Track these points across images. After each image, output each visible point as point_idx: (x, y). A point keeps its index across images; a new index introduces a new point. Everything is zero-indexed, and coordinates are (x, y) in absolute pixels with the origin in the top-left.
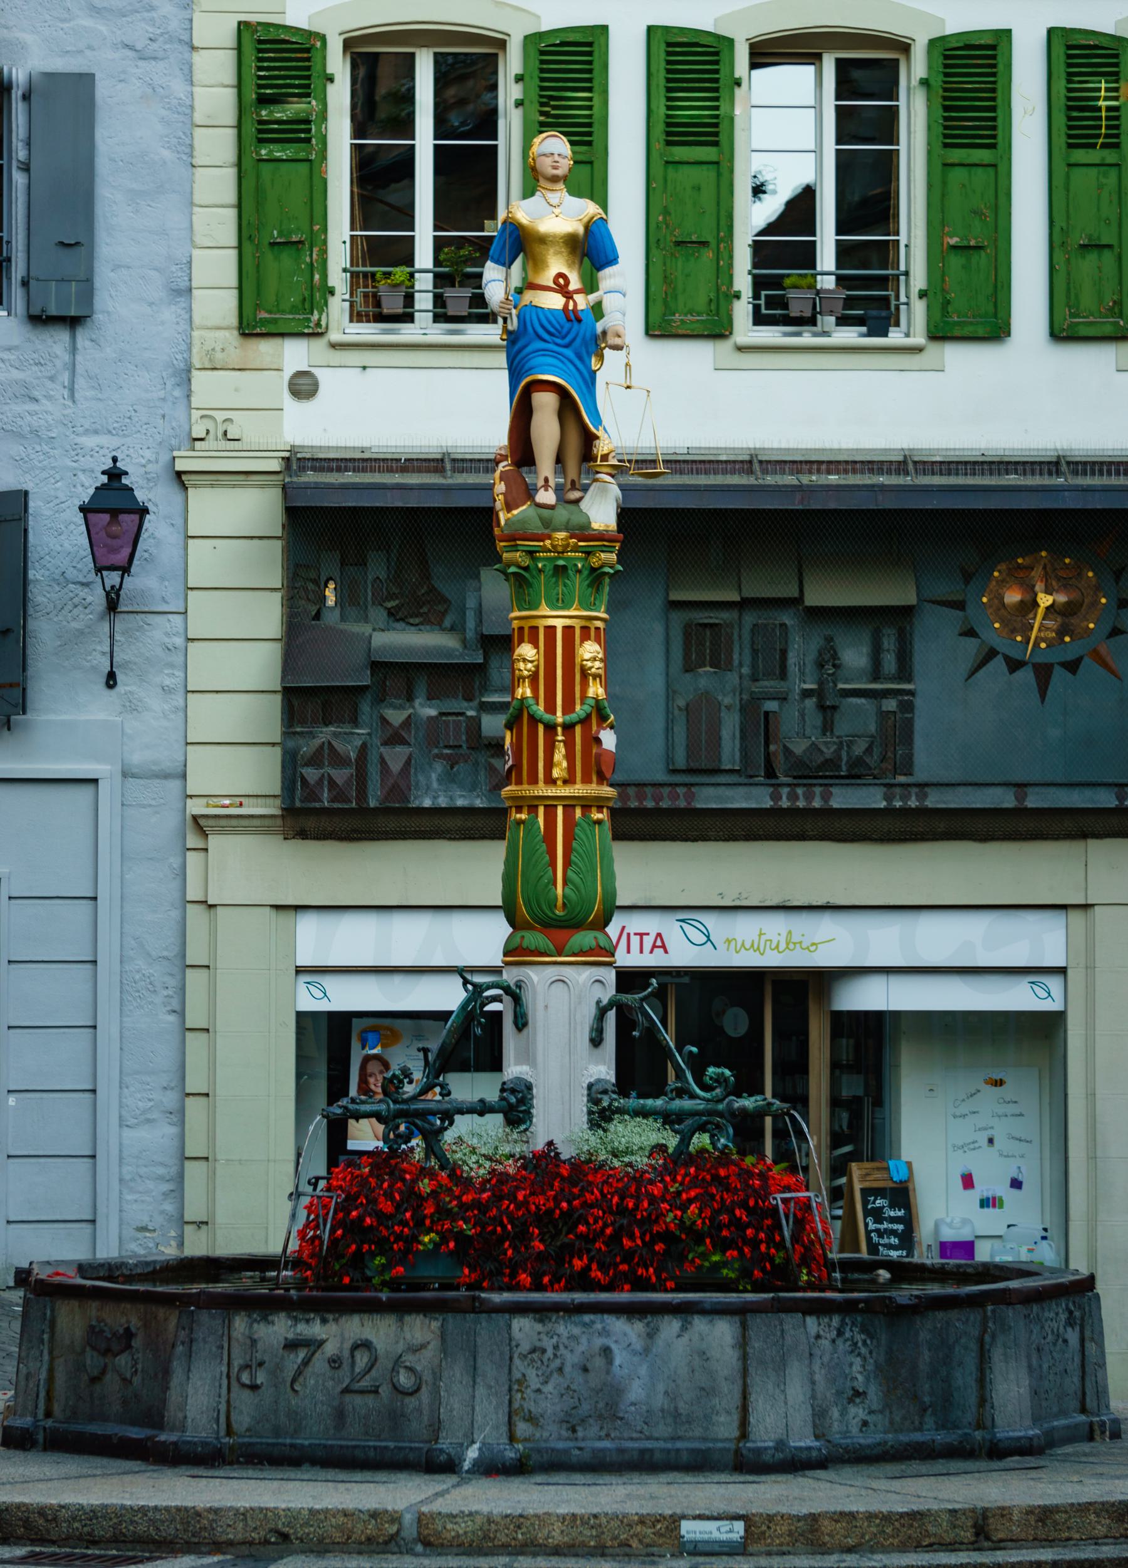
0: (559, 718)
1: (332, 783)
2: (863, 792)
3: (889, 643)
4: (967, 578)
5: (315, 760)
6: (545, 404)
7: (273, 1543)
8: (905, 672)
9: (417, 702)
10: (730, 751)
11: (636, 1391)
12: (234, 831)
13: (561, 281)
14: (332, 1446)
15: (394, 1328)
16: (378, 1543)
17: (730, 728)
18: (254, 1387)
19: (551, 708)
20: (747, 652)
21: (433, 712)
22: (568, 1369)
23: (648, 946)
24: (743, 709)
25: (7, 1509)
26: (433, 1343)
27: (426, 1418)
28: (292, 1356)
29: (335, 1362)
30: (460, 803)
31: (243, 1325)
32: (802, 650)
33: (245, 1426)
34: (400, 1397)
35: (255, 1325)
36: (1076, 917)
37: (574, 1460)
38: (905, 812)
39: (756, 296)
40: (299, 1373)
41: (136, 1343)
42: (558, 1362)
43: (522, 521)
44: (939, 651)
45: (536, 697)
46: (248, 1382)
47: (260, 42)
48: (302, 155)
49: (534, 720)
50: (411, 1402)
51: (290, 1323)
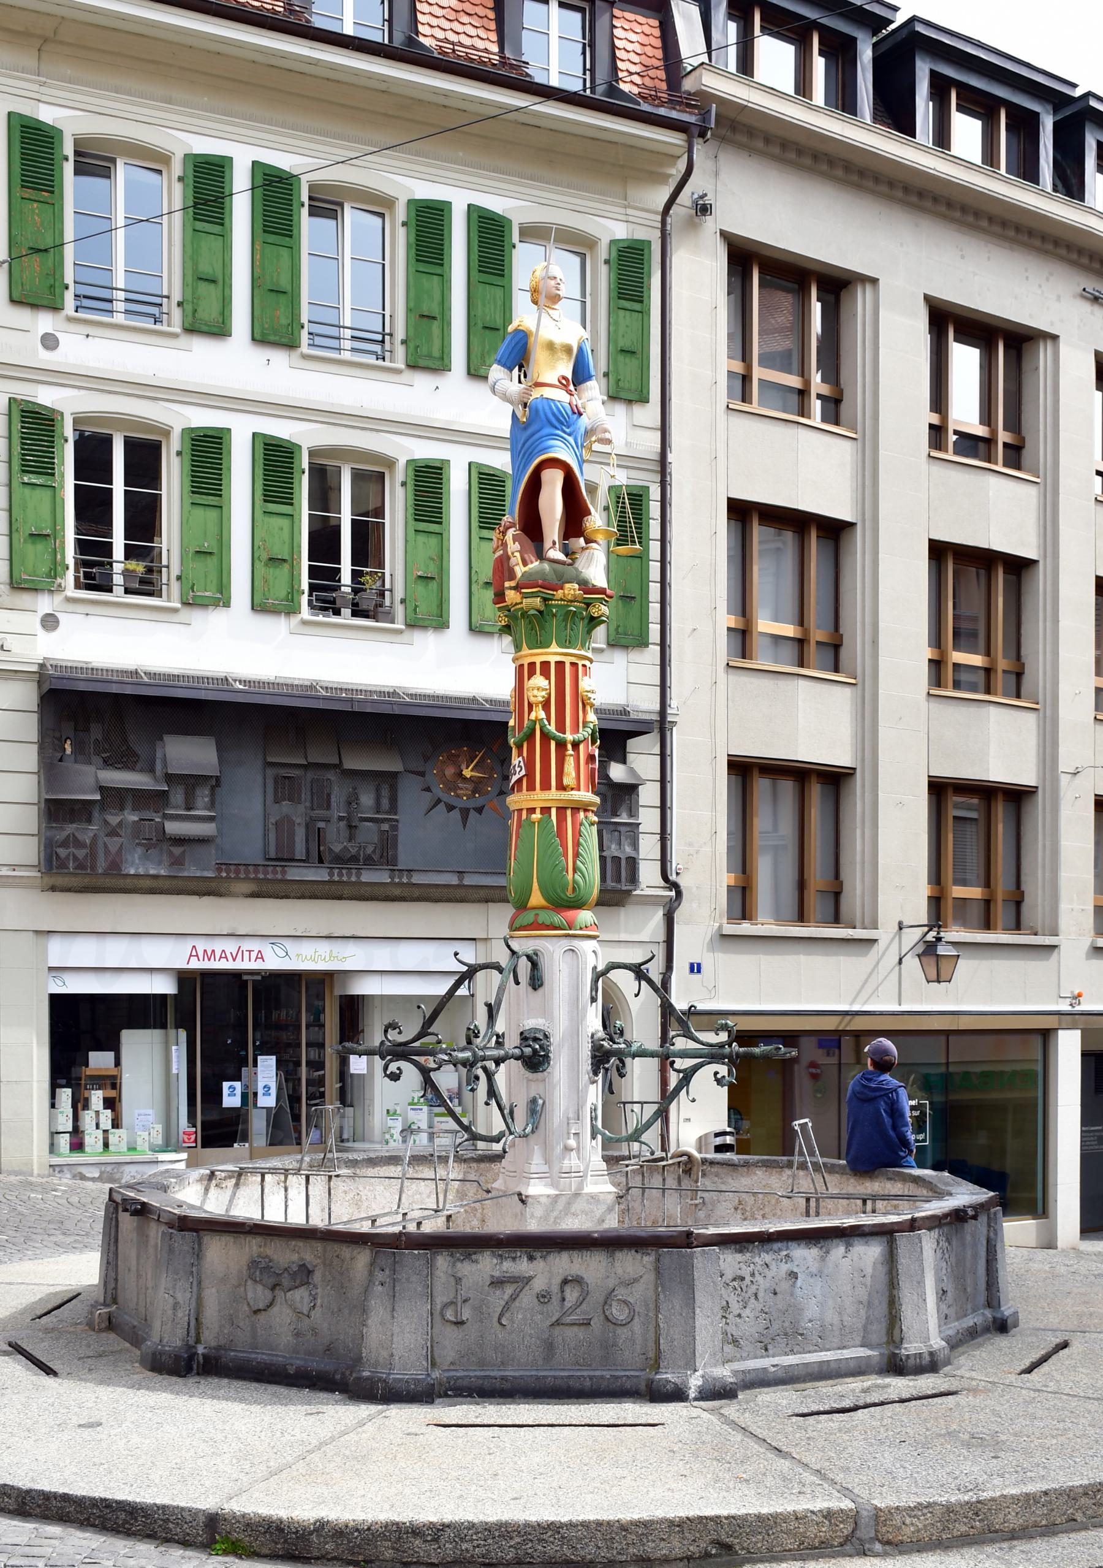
0: (569, 737)
1: (75, 858)
2: (378, 873)
3: (385, 792)
4: (426, 759)
5: (65, 844)
6: (553, 481)
7: (715, 1556)
8: (393, 808)
9: (126, 812)
10: (300, 851)
11: (812, 1310)
12: (10, 886)
13: (564, 382)
14: (545, 1377)
15: (604, 1263)
16: (832, 1546)
17: (300, 835)
18: (460, 1323)
19: (561, 727)
20: (309, 793)
21: (136, 819)
22: (761, 1295)
23: (253, 957)
24: (307, 826)
25: (369, 1529)
26: (645, 1277)
27: (638, 1347)
28: (498, 1292)
29: (543, 1297)
30: (152, 872)
31: (446, 1264)
32: (338, 794)
33: (450, 1359)
34: (612, 1326)
35: (459, 1265)
36: (480, 945)
37: (771, 1376)
38: (401, 884)
39: (310, 595)
40: (507, 1307)
41: (317, 1277)
42: (754, 1288)
43: (541, 573)
44: (412, 798)
45: (549, 720)
46: (453, 1319)
47: (23, 411)
48: (49, 483)
49: (546, 737)
50: (623, 1333)
51: (495, 1261)
